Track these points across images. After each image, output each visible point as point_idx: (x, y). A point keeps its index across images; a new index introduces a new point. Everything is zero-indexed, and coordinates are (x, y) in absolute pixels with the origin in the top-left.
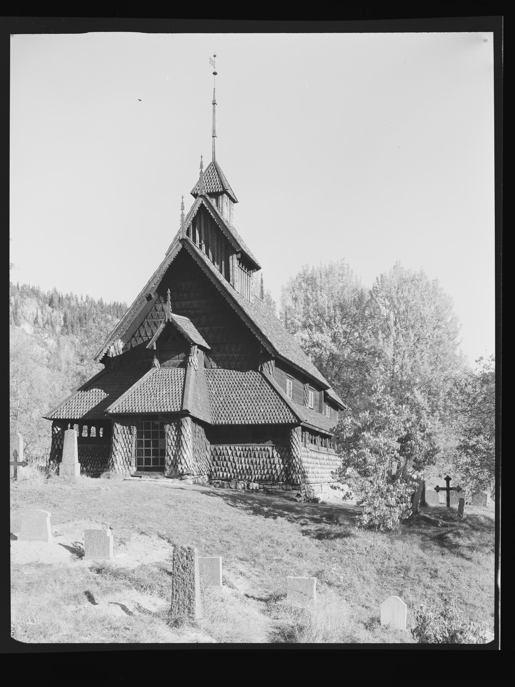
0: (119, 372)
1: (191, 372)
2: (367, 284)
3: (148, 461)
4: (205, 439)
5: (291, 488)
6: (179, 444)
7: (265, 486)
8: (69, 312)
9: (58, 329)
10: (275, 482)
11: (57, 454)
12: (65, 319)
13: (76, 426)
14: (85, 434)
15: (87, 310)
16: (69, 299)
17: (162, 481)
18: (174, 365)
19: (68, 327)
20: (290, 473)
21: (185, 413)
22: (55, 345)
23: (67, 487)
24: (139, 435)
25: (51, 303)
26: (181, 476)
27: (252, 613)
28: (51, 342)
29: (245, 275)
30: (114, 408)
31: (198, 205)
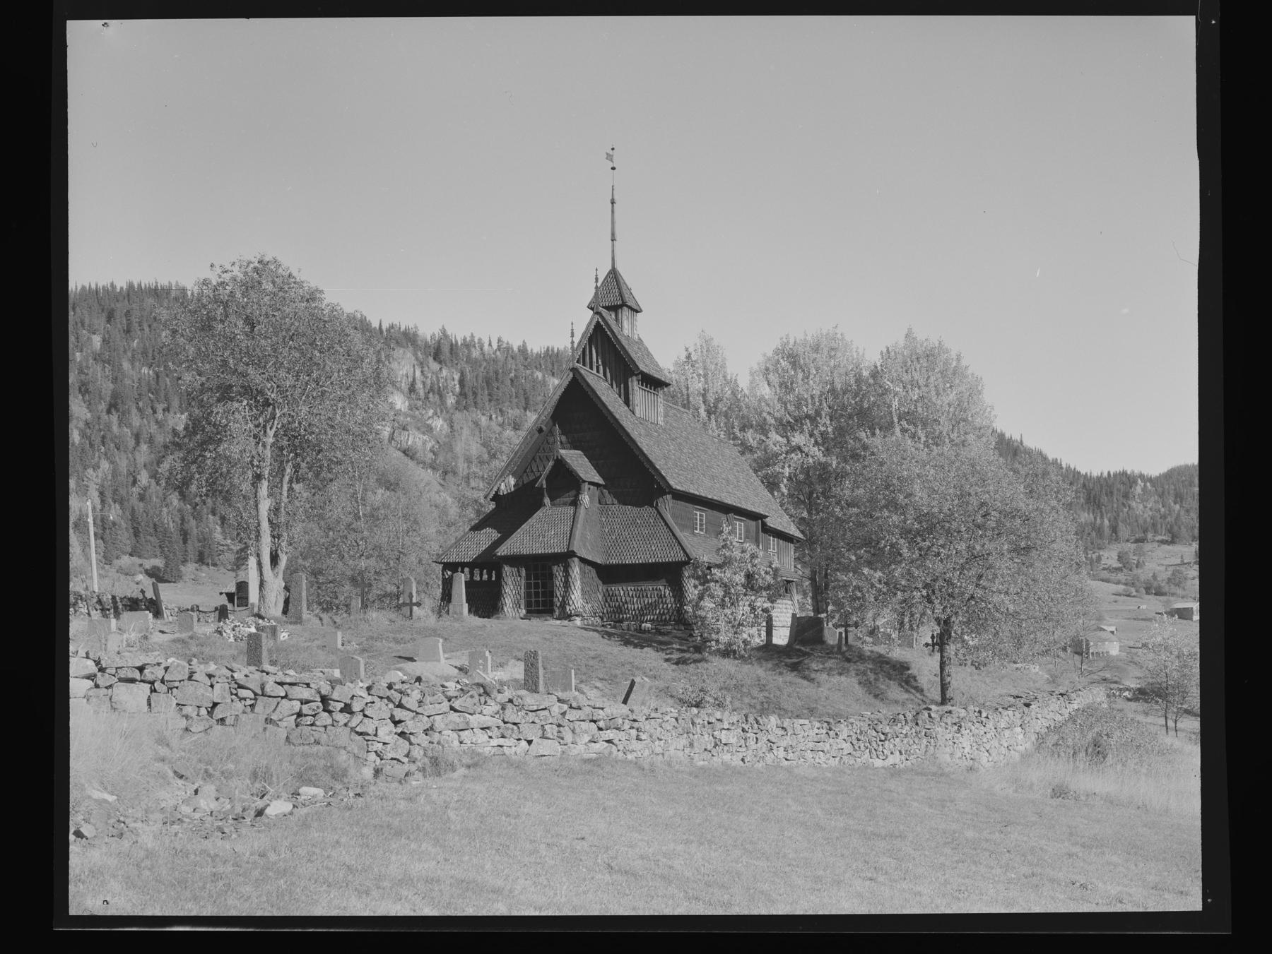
0: (509, 511)
1: (582, 511)
2: (871, 357)
3: (537, 603)
4: (597, 579)
6: (567, 585)
8: (468, 369)
9: (451, 400)
10: (666, 623)
11: (447, 596)
12: (462, 382)
13: (466, 570)
14: (477, 578)
15: (500, 364)
16: (468, 345)
17: (552, 624)
18: (565, 504)
19: (467, 398)
21: (571, 554)
22: (446, 428)
23: (457, 625)
24: (528, 578)
25: (437, 356)
26: (569, 617)
27: (333, 448)
28: (439, 424)
30: (502, 551)
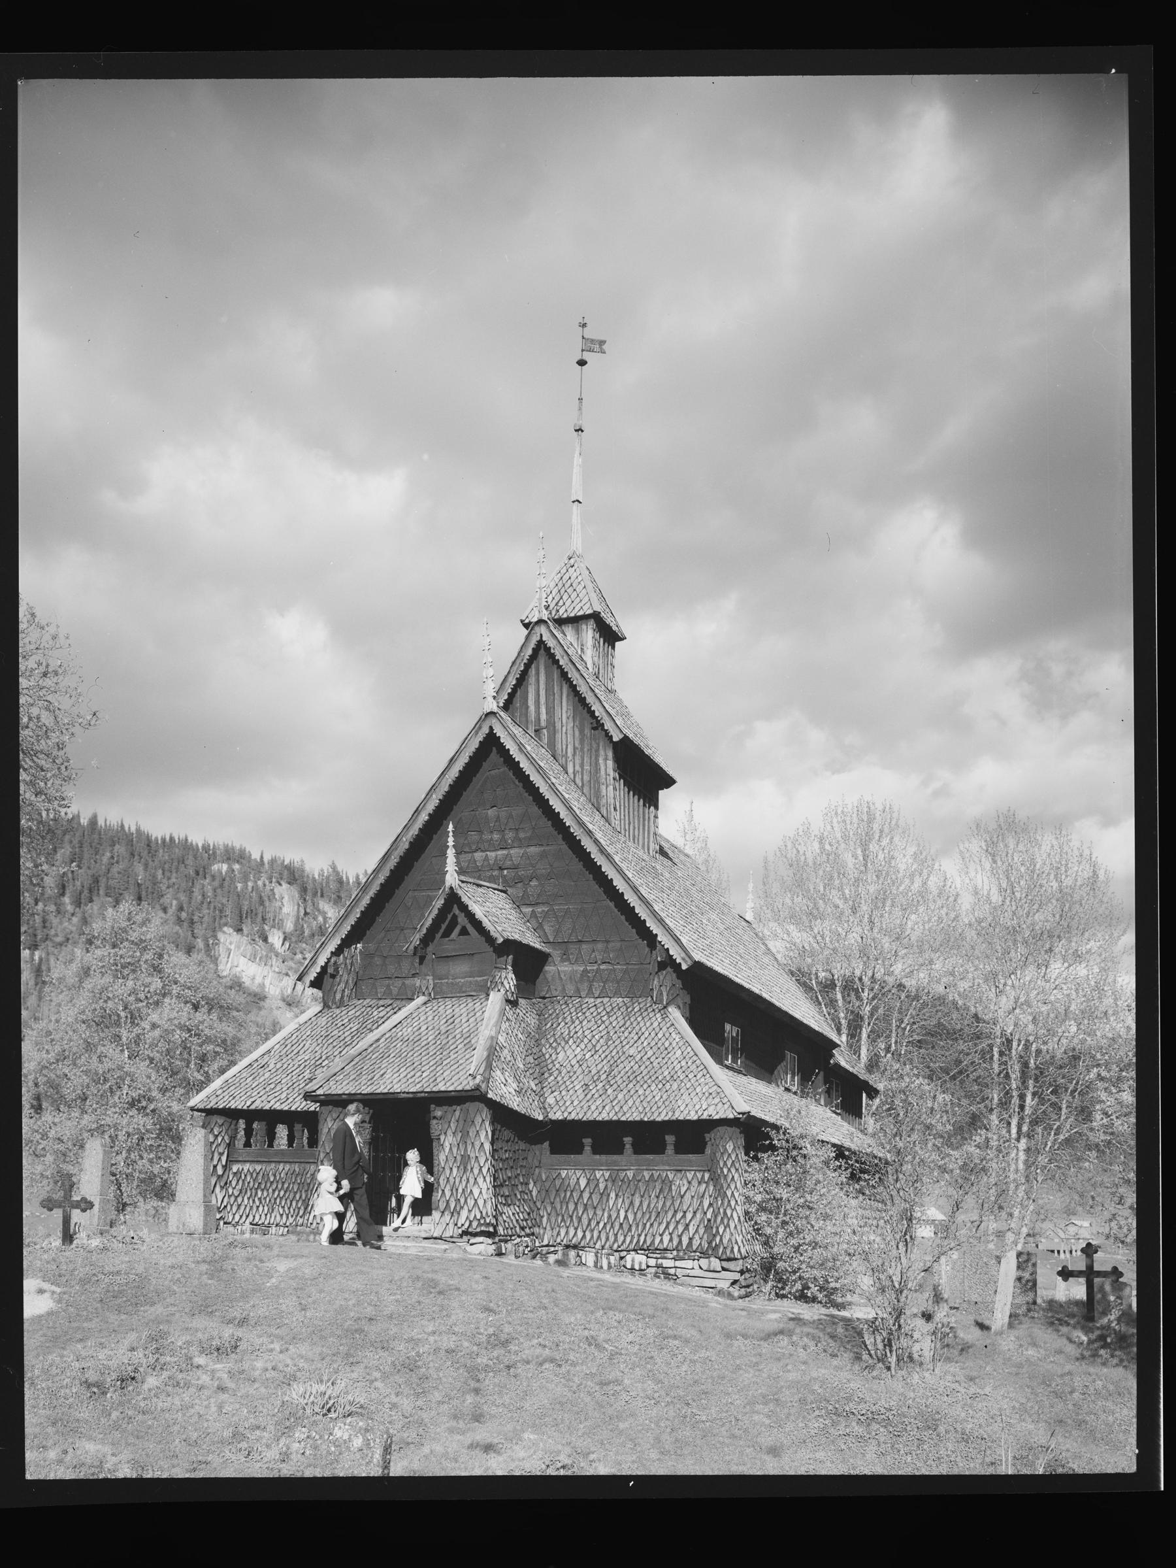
7: (660, 1261)
20: (718, 1231)
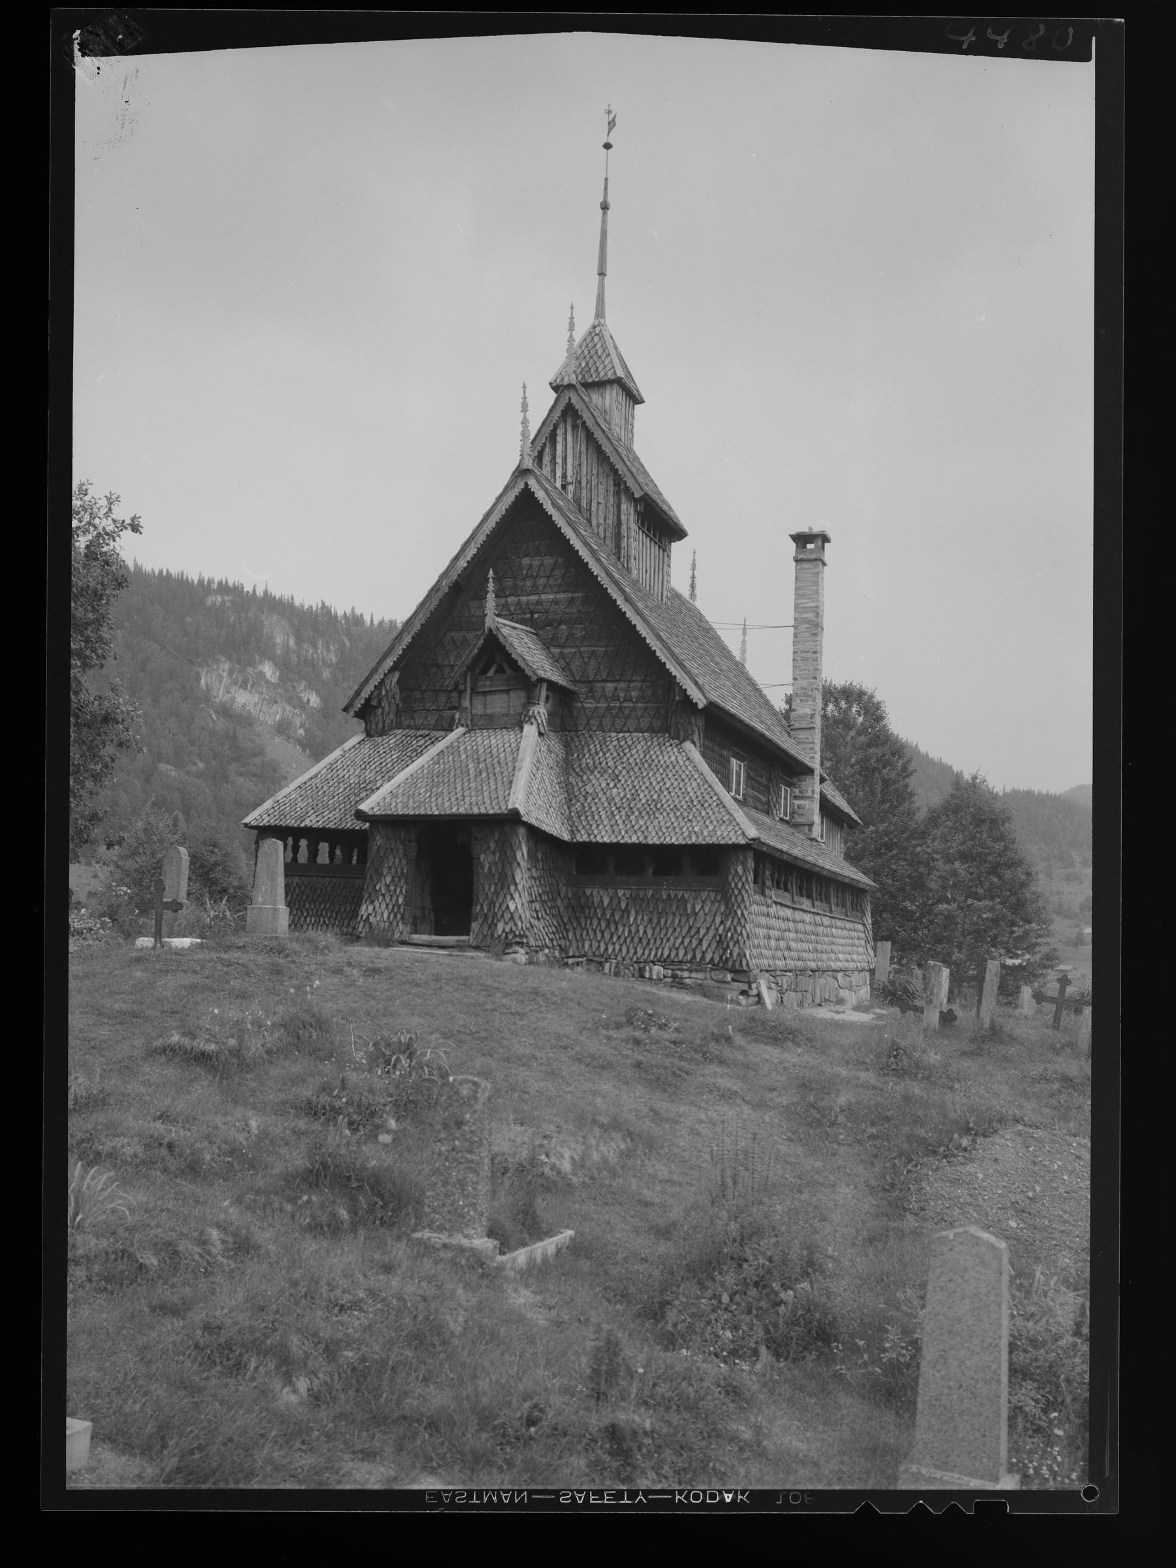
5: (729, 977)
29: (655, 549)
31: (561, 406)
